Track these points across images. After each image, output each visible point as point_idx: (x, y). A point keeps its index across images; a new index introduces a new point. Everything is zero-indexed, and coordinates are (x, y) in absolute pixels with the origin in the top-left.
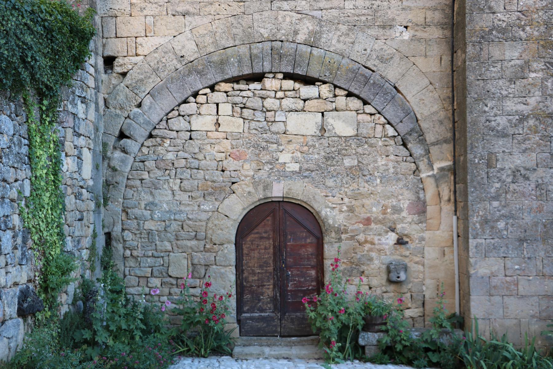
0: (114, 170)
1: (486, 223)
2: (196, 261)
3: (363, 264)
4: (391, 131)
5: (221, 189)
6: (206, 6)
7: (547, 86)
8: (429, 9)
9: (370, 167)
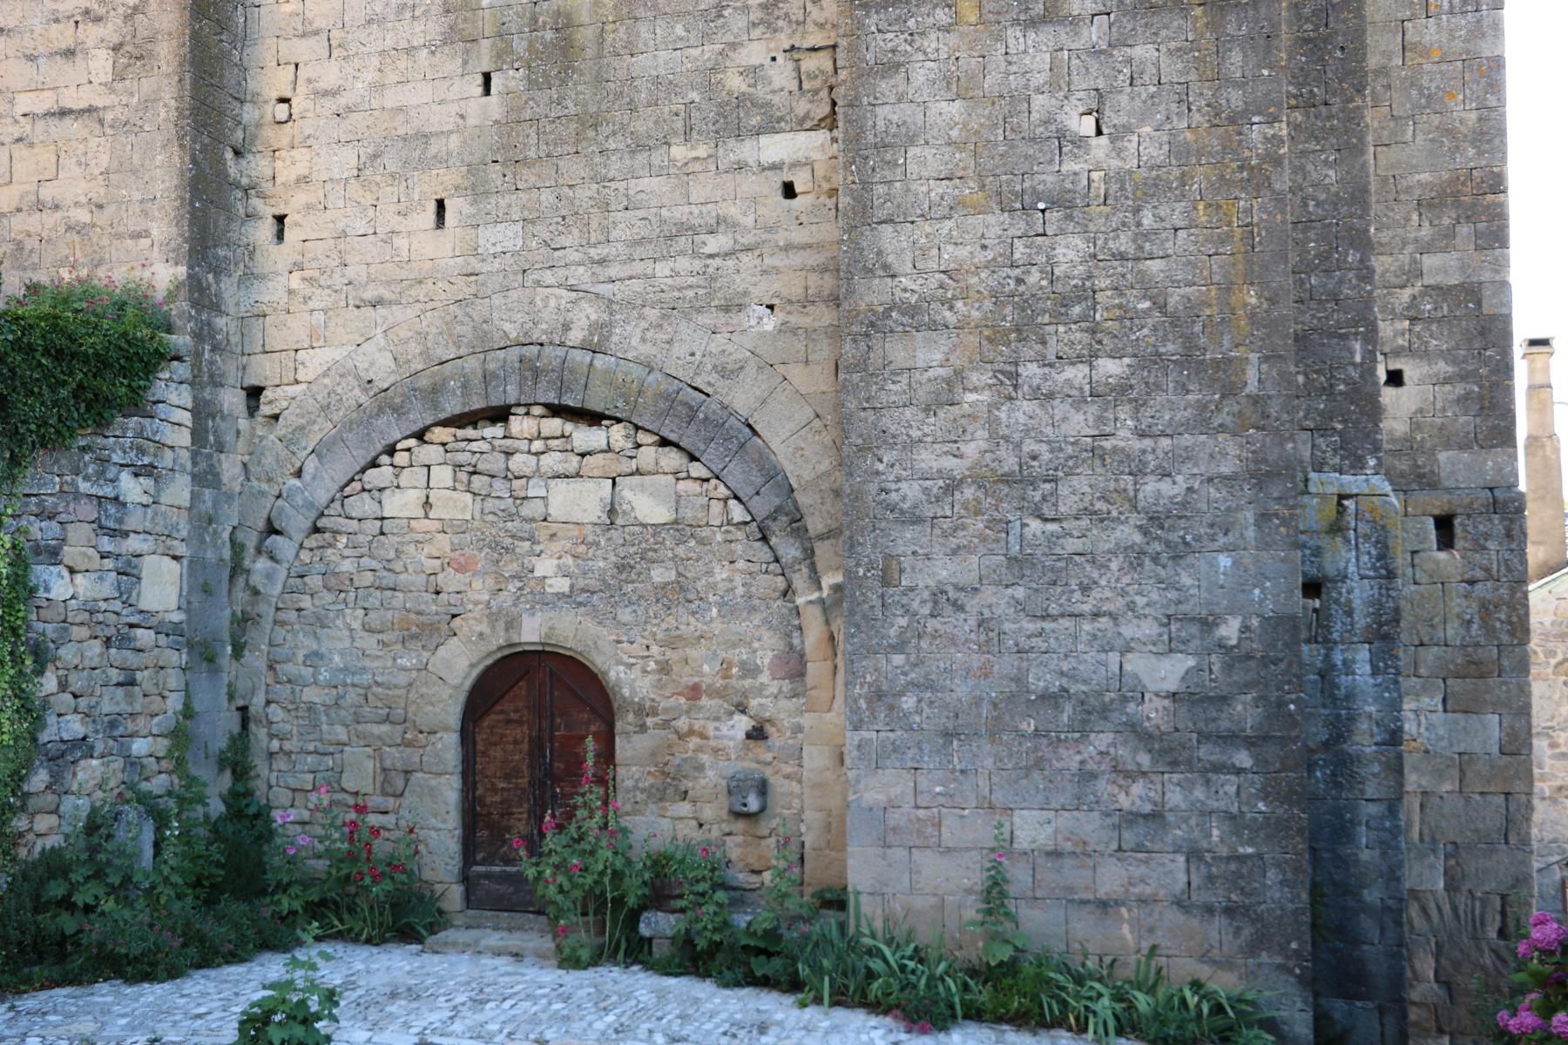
0: (256, 592)
1: (880, 698)
2: (388, 764)
3: (685, 777)
4: (737, 512)
5: (433, 628)
6: (411, 286)
7: (998, 419)
8: (813, 270)
9: (699, 585)
